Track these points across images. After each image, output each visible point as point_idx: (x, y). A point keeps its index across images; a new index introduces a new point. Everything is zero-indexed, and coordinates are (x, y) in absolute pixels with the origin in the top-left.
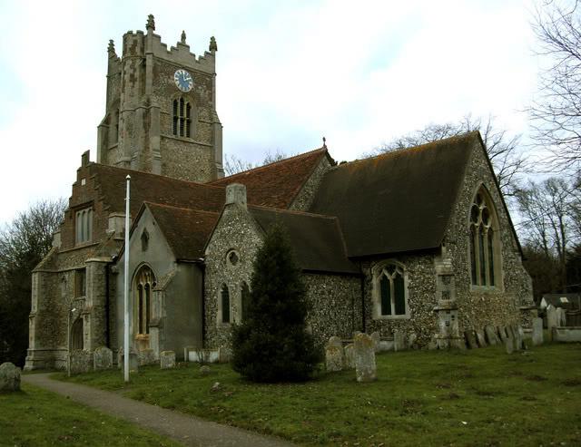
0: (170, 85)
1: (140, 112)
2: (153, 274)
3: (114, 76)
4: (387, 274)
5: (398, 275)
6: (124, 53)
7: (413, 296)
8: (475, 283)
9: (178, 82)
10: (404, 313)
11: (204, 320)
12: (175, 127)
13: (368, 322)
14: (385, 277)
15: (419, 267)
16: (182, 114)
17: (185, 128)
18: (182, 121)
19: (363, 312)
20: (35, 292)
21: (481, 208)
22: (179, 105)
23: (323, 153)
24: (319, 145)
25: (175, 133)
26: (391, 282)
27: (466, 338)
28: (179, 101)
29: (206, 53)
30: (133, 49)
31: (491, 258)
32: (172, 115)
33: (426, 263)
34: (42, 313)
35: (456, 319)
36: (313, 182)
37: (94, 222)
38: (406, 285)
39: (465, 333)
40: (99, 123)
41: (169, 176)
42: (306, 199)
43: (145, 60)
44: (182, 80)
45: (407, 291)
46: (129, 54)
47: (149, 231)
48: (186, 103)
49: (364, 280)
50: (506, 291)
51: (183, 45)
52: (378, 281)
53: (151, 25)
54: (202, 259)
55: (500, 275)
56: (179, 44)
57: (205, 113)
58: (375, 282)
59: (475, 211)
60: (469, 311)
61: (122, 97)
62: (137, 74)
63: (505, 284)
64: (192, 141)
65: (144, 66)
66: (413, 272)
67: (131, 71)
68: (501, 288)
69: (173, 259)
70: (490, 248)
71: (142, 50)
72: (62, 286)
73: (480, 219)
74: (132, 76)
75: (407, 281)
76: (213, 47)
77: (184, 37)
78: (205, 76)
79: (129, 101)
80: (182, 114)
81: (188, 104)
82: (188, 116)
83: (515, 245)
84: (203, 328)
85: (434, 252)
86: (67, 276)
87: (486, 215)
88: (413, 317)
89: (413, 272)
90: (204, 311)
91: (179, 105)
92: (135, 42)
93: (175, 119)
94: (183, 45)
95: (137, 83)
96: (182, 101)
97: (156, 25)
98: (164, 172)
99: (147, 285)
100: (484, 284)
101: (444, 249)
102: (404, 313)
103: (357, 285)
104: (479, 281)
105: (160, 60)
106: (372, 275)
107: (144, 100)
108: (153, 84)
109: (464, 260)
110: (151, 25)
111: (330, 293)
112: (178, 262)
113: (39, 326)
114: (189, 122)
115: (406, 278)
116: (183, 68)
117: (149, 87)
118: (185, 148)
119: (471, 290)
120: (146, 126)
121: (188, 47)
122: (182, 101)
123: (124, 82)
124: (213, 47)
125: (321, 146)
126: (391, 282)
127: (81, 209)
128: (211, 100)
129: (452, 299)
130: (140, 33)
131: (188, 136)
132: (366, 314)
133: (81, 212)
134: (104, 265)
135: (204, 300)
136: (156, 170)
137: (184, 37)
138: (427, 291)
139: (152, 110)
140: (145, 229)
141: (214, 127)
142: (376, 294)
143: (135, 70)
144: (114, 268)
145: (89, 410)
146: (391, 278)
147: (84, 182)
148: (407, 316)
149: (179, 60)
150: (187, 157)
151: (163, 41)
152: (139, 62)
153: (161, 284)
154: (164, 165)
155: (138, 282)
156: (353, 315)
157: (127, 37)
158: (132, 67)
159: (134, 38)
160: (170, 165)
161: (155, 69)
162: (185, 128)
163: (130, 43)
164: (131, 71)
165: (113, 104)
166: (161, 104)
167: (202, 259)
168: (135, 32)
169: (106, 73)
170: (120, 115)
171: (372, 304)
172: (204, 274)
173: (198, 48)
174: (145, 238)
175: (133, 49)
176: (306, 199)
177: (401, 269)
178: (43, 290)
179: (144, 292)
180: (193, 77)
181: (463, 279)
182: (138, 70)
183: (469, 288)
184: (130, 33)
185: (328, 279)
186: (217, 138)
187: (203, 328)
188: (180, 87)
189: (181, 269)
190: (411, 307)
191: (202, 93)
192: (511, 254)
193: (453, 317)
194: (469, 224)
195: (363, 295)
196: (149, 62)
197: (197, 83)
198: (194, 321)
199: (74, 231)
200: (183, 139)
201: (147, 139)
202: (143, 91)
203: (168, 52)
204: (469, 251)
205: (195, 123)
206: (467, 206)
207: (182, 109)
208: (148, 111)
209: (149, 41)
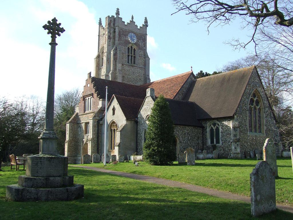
2: (116, 125)
4: (213, 126)
5: (217, 127)
7: (223, 136)
8: (251, 131)
9: (130, 39)
11: (137, 144)
13: (205, 147)
16: (131, 53)
17: (133, 60)
18: (131, 56)
19: (203, 142)
20: (68, 133)
21: (255, 99)
22: (130, 49)
25: (128, 62)
27: (245, 154)
28: (130, 48)
31: (260, 121)
32: (127, 54)
35: (239, 146)
37: (93, 102)
38: (220, 131)
39: (244, 152)
42: (183, 94)
43: (115, 29)
44: (132, 39)
45: (220, 134)
48: (133, 48)
49: (203, 128)
50: (266, 135)
51: (132, 22)
52: (209, 130)
53: (118, 13)
54: (137, 119)
56: (131, 21)
57: (142, 53)
58: (208, 130)
59: (252, 101)
62: (112, 36)
63: (266, 132)
64: (136, 65)
65: (115, 32)
70: (260, 117)
71: (114, 24)
73: (254, 104)
75: (221, 130)
76: (146, 22)
77: (133, 18)
78: (142, 36)
80: (131, 53)
81: (134, 49)
82: (134, 54)
83: (272, 115)
84: (137, 147)
87: (257, 103)
88: (222, 145)
90: (137, 140)
91: (130, 49)
93: (128, 56)
94: (132, 22)
95: (112, 40)
96: (131, 47)
97: (120, 13)
98: (123, 80)
99: (114, 129)
100: (256, 131)
102: (219, 143)
103: (200, 130)
104: (253, 130)
106: (207, 127)
108: (119, 40)
110: (118, 13)
111: (188, 134)
114: (134, 57)
115: (220, 128)
117: (117, 42)
118: (132, 69)
119: (248, 134)
122: (131, 47)
124: (146, 22)
126: (214, 130)
127: (87, 97)
128: (144, 47)
129: (238, 137)
130: (113, 16)
131: (134, 63)
132: (204, 142)
134: (97, 121)
135: (137, 136)
136: (119, 80)
137: (133, 18)
138: (228, 134)
140: (114, 106)
143: (111, 34)
144: (101, 122)
145: (192, 192)
146: (214, 128)
148: (220, 144)
150: (133, 73)
151: (123, 20)
153: (120, 129)
154: (123, 77)
156: (198, 144)
159: (110, 19)
160: (126, 77)
162: (133, 60)
167: (137, 119)
168: (111, 16)
170: (104, 54)
171: (207, 139)
172: (137, 125)
173: (139, 23)
174: (114, 110)
176: (183, 94)
177: (218, 125)
178: (71, 131)
179: (113, 132)
180: (137, 36)
181: (244, 130)
182: (112, 34)
183: (247, 133)
187: (137, 147)
188: (131, 41)
191: (140, 44)
192: (270, 119)
193: (238, 145)
196: (117, 30)
198: (133, 144)
202: (114, 44)
205: (137, 57)
206: (248, 98)
207: (131, 51)
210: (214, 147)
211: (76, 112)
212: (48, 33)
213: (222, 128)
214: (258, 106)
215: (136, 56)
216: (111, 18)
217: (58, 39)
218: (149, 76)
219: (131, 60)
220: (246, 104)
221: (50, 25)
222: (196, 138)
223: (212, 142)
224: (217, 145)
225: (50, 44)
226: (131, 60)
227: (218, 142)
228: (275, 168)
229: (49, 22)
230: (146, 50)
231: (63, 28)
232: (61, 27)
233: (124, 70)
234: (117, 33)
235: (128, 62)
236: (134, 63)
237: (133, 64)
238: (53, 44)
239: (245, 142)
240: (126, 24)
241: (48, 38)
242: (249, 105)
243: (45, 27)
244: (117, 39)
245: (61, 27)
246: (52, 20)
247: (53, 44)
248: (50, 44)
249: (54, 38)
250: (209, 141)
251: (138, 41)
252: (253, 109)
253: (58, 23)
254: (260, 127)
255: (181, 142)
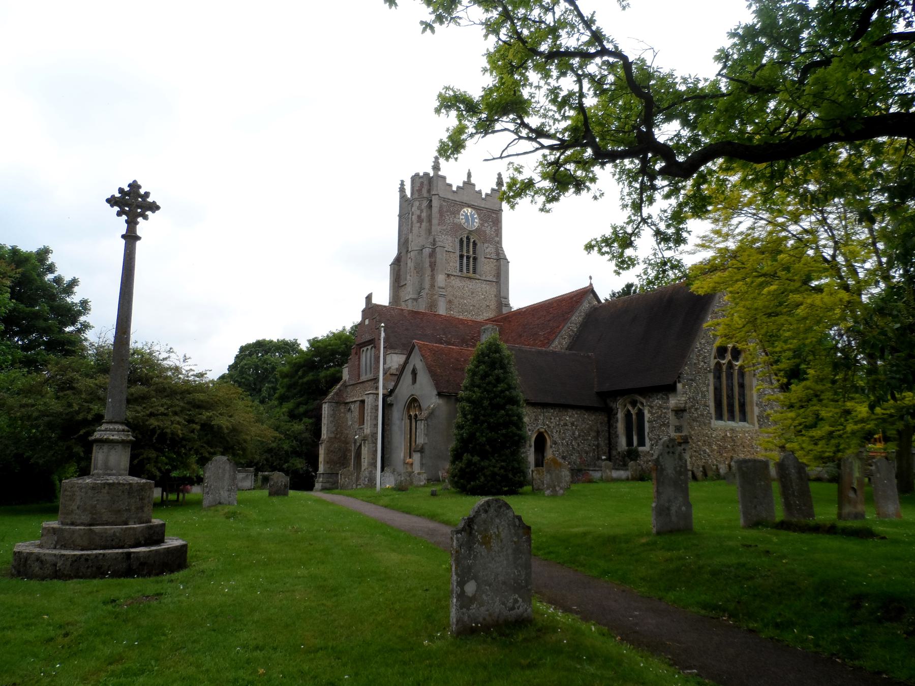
0: (456, 224)
1: (427, 251)
3: (403, 216)
4: (630, 408)
6: (412, 194)
7: (652, 429)
8: (720, 417)
10: (644, 445)
12: (461, 264)
13: (614, 453)
14: (629, 411)
15: (658, 402)
16: (468, 251)
18: (468, 258)
21: (730, 345)
22: (465, 243)
23: (589, 291)
24: (585, 284)
25: (461, 270)
26: (634, 417)
28: (465, 239)
29: (493, 190)
30: (420, 191)
31: (742, 395)
32: (458, 253)
33: (663, 398)
34: (331, 440)
36: (577, 318)
38: (646, 419)
39: (703, 467)
40: (391, 260)
41: (454, 313)
42: (570, 336)
43: (431, 201)
44: (468, 217)
45: (647, 425)
46: (416, 196)
47: (417, 367)
48: (472, 240)
49: (610, 414)
51: (468, 184)
55: (752, 412)
58: (620, 415)
60: (710, 445)
61: (410, 237)
62: (424, 215)
63: (759, 420)
64: (478, 277)
65: (430, 206)
66: (652, 407)
67: (418, 212)
68: (754, 425)
69: (435, 392)
71: (429, 191)
72: (349, 415)
73: (729, 356)
74: (419, 217)
75: (647, 415)
77: (469, 175)
79: (415, 243)
80: (468, 251)
81: (474, 242)
82: (474, 252)
85: (671, 389)
86: (352, 406)
88: (652, 449)
89: (652, 407)
91: (465, 243)
92: (422, 183)
93: (461, 257)
94: (468, 184)
95: (424, 224)
96: (468, 238)
99: (416, 415)
100: (732, 418)
101: (679, 386)
102: (644, 445)
103: (602, 418)
105: (444, 199)
107: (431, 240)
109: (704, 396)
111: (573, 424)
112: (440, 394)
113: (329, 452)
114: (475, 259)
115: (646, 412)
116: (469, 206)
117: (436, 228)
118: (471, 285)
119: (712, 425)
120: (433, 266)
121: (474, 185)
122: (468, 238)
123: (412, 223)
125: (587, 284)
126: (634, 417)
130: (426, 174)
131: (474, 272)
132: (611, 444)
133: (365, 349)
137: (469, 175)
138: (664, 425)
139: (437, 249)
141: (500, 261)
142: (620, 427)
143: (422, 211)
146: (633, 412)
147: (367, 322)
149: (465, 199)
150: (472, 293)
151: (448, 181)
152: (425, 203)
153: (425, 414)
155: (408, 412)
156: (598, 446)
157: (415, 178)
158: (419, 208)
160: (456, 301)
161: (441, 212)
163: (418, 185)
164: (418, 212)
165: (403, 243)
166: (449, 243)
168: (421, 174)
169: (398, 213)
171: (617, 436)
174: (414, 373)
175: (420, 191)
176: (570, 336)
177: (642, 404)
179: (413, 421)
181: (702, 415)
183: (710, 423)
184: (417, 175)
185: (570, 412)
186: (502, 273)
189: (440, 401)
190: (651, 440)
191: (488, 230)
194: (713, 362)
195: (609, 428)
196: (436, 203)
197: (483, 220)
199: (359, 365)
200: (469, 275)
201: (433, 278)
202: (429, 231)
203: (454, 192)
204: (711, 388)
205: (481, 260)
207: (468, 246)
208: (434, 251)
209: (435, 182)
210: (632, 454)
211: (344, 378)
212: (119, 214)
213: (649, 412)
214: (737, 361)
215: (479, 257)
216: (422, 177)
217: (143, 227)
218: (507, 298)
219: (468, 265)
220: (705, 357)
221: (123, 198)
222: (593, 434)
223: (630, 442)
224: (641, 449)
225: (139, 238)
226: (468, 265)
227: (642, 443)
228: (684, 508)
229: (121, 190)
230: (499, 242)
231: (112, 206)
232: (150, 200)
233: (453, 287)
234: (435, 210)
235: (461, 270)
236: (474, 272)
237: (471, 275)
238: (131, 238)
239: (704, 444)
240: (454, 189)
241: (121, 224)
242: (715, 358)
243: (112, 201)
244: (435, 221)
245: (150, 200)
246: (129, 186)
247: (131, 238)
248: (139, 238)
249: (132, 224)
250: (622, 441)
251: (482, 225)
252: (724, 367)
253: (142, 191)
254: (742, 406)
255: (555, 443)
